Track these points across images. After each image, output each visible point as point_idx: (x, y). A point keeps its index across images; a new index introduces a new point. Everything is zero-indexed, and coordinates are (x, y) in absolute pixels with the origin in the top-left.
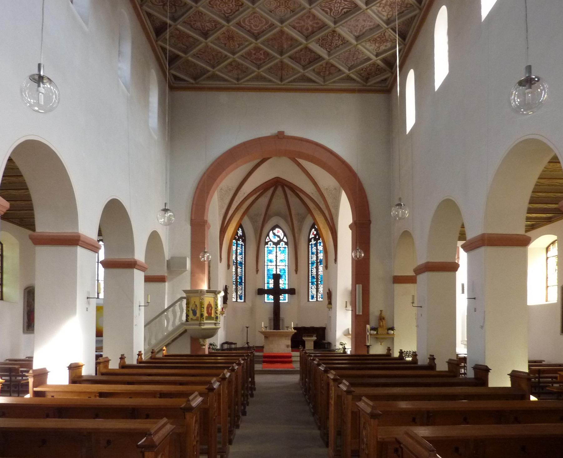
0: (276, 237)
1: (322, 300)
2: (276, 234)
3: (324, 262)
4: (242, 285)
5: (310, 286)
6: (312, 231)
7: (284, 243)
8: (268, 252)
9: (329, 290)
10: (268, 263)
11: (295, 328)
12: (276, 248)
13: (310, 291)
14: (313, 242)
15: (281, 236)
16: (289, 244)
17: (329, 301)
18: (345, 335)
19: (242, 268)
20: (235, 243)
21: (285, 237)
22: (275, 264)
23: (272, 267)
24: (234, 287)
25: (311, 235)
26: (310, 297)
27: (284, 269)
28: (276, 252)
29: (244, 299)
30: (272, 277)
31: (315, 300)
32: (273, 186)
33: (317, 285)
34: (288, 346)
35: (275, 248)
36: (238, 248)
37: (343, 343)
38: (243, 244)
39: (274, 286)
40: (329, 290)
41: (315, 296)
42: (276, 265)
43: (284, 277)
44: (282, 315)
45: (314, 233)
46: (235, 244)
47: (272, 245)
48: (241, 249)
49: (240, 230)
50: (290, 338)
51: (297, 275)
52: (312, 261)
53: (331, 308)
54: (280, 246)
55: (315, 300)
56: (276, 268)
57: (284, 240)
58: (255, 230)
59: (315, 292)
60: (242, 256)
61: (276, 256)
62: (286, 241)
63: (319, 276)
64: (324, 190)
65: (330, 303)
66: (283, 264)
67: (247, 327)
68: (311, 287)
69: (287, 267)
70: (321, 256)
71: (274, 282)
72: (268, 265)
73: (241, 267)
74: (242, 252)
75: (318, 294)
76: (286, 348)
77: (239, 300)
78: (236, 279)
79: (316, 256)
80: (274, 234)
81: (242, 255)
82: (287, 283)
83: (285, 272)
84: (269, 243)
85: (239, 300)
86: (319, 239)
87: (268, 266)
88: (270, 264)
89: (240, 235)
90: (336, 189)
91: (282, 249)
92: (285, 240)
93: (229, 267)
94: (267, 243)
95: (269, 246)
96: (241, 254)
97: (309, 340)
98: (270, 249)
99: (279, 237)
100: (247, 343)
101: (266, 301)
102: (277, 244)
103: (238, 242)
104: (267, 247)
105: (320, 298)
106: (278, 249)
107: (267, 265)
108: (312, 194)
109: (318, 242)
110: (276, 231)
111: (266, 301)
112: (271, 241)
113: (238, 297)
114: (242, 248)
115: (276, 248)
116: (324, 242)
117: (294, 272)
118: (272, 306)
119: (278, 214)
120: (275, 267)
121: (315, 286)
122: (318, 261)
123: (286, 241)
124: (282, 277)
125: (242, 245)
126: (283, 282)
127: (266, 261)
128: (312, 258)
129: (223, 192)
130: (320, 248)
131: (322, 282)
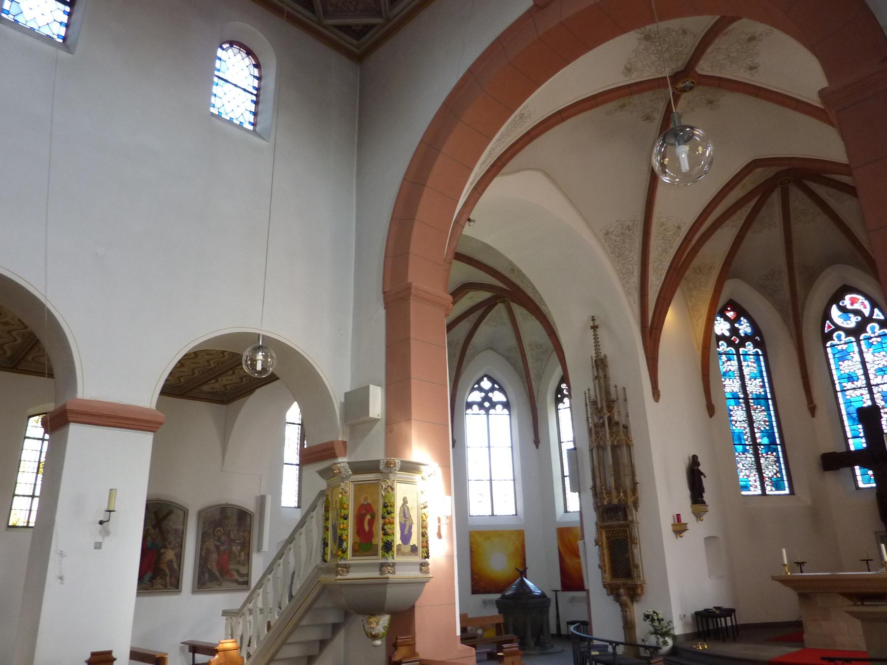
0: (851, 315)
2: (849, 307)
4: (776, 450)
8: (837, 356)
22: (864, 382)
23: (858, 392)
28: (861, 353)
35: (855, 344)
42: (869, 386)
48: (755, 365)
54: (869, 333)
56: (871, 393)
57: (874, 317)
61: (864, 363)
72: (845, 389)
77: (770, 490)
80: (843, 310)
82: (849, 440)
85: (770, 490)
87: (847, 393)
88: (849, 385)
92: (878, 315)
94: (828, 337)
98: (839, 348)
99: (857, 312)
102: (856, 332)
104: (832, 346)
106: (862, 343)
110: (847, 302)
112: (838, 328)
120: (865, 391)
125: (757, 354)
127: (837, 382)
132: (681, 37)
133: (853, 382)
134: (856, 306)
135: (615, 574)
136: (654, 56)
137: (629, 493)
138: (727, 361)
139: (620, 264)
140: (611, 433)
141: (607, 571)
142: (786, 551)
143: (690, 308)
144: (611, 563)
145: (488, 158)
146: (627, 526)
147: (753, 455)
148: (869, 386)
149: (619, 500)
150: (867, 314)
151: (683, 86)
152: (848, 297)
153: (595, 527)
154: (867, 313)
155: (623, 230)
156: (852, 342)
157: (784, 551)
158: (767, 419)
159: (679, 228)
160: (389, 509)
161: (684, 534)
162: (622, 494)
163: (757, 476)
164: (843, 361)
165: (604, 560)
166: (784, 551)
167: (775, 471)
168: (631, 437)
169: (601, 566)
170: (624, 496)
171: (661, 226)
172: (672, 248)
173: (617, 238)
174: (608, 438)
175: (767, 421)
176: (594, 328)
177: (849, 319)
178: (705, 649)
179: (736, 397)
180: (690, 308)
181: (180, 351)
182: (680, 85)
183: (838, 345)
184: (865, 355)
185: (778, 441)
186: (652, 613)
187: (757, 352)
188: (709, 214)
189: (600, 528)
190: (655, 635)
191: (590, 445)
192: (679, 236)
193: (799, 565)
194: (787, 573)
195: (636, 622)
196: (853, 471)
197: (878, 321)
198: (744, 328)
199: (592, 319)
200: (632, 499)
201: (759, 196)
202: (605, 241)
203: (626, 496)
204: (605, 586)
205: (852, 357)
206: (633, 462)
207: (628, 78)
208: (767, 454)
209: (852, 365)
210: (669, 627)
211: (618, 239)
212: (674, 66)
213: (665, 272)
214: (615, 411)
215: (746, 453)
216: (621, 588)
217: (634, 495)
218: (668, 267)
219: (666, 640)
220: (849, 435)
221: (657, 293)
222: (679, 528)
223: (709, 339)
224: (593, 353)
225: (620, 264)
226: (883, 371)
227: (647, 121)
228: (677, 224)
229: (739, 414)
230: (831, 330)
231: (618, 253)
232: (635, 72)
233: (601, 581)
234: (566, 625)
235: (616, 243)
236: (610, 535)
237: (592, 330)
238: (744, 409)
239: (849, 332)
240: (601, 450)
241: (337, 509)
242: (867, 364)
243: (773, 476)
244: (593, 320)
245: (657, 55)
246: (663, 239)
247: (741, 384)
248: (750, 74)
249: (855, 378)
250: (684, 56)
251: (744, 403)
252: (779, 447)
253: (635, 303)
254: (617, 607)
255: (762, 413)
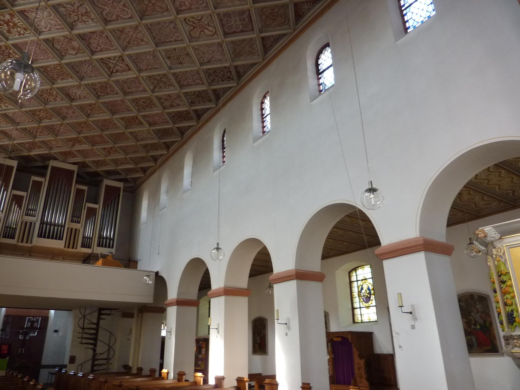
160: (504, 278)
181: (423, 193)
219: (99, 260)
234: (317, 86)
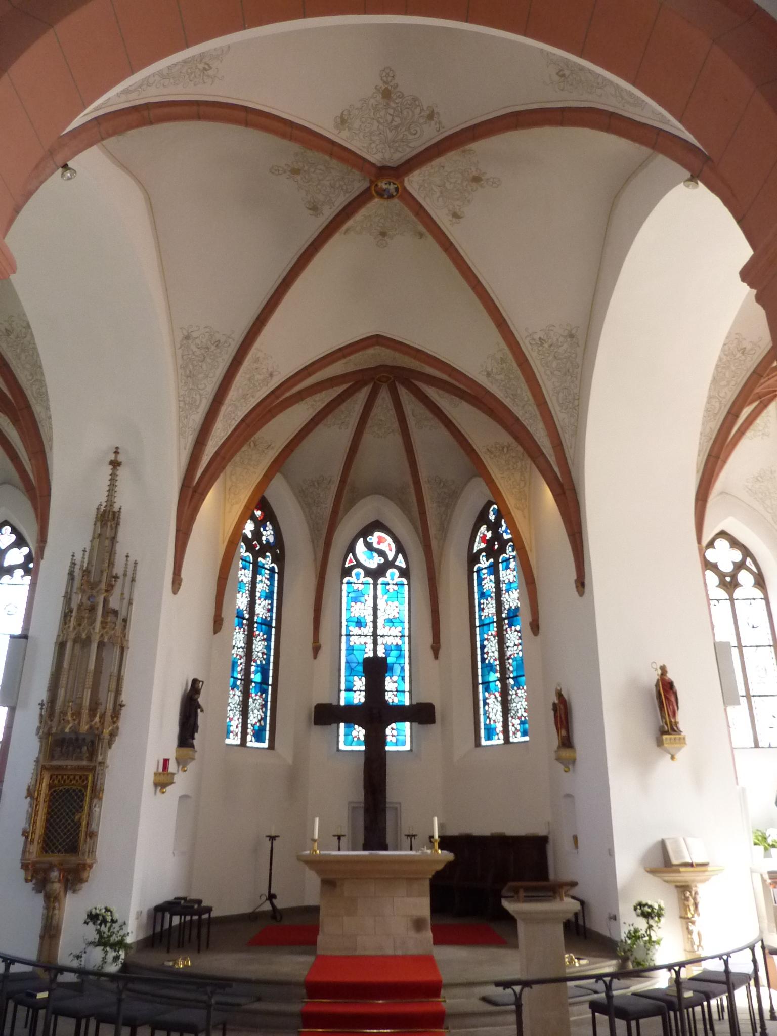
0: (375, 555)
1: (527, 738)
2: (375, 545)
3: (525, 618)
4: (265, 691)
5: (481, 697)
6: (479, 534)
7: (396, 572)
8: (351, 595)
9: (560, 695)
10: (351, 628)
11: (446, 842)
12: (375, 585)
13: (481, 711)
14: (484, 563)
15: (388, 552)
16: (414, 573)
17: (564, 733)
18: (653, 871)
19: (268, 640)
20: (250, 563)
21: (400, 556)
22: (371, 630)
23: (363, 640)
24: (235, 697)
25: (476, 544)
26: (482, 733)
27: (398, 647)
28: (375, 598)
29: (269, 740)
30: (360, 668)
31: (501, 741)
32: (365, 384)
33: (505, 692)
34: (418, 924)
35: (372, 586)
36: (259, 577)
37: (650, 907)
38: (276, 570)
39: (366, 697)
40: (560, 695)
41: (499, 727)
42: (375, 635)
43: (397, 669)
44: (395, 792)
45: (485, 536)
46: (251, 565)
47: (362, 579)
48: (268, 583)
49: (267, 528)
50: (427, 883)
51: (437, 662)
52: (483, 618)
53: (574, 761)
54: (387, 579)
55: (498, 740)
56: (375, 643)
57: (397, 563)
58: (314, 528)
59: (500, 714)
60: (270, 602)
61: (375, 609)
62: (403, 565)
63: (510, 661)
64: (530, 347)
65: (567, 742)
66: (396, 631)
67: (272, 838)
68: (485, 700)
69: (406, 639)
70: (512, 599)
71: (366, 686)
72: (351, 633)
73: (265, 636)
74: (272, 592)
75: (510, 719)
76: (412, 933)
77: (251, 743)
78: (247, 671)
79: (494, 602)
80: (369, 546)
81: (272, 599)
82: (408, 690)
83: (400, 656)
84: (354, 572)
85: (251, 743)
86: (503, 550)
87: (352, 639)
88: (355, 630)
89: (267, 541)
90: (571, 336)
91: (391, 587)
92: (401, 562)
93: (180, 585)
94: (347, 572)
95: (353, 579)
96: (269, 596)
97: (534, 919)
98: (355, 587)
99: (381, 553)
100: (271, 897)
101: (342, 747)
102: (376, 574)
103: (260, 559)
104: (349, 583)
105: (519, 734)
106: (379, 587)
107: (348, 635)
108: (488, 375)
109: (500, 561)
110: (374, 539)
111: (342, 747)
112: (359, 565)
113: (249, 731)
114: (271, 579)
115: (375, 585)
116: (519, 546)
117: (431, 653)
118: (361, 761)
119: (379, 489)
120: (370, 640)
121: (497, 694)
122: (504, 615)
123: (403, 565)
124: (392, 669)
125: (272, 570)
126: (396, 685)
127: (344, 623)
128: (482, 610)
129: (195, 349)
130: (508, 575)
131: (523, 679)
132: (421, 121)
133: (360, 628)
134: (383, 547)
135: (48, 845)
136: (377, 124)
137: (108, 719)
138: (242, 568)
139: (186, 388)
140: (104, 624)
141: (36, 843)
142: (438, 820)
143: (228, 487)
144: (46, 828)
145: (135, 90)
146: (93, 770)
147: (242, 693)
148: (375, 635)
149: (91, 728)
150: (391, 558)
151: (385, 186)
152: (377, 534)
153: (34, 767)
154: (391, 556)
155: (209, 342)
156: (369, 584)
157: (317, 820)
158: (265, 651)
159: (271, 375)
161: (168, 789)
162: (97, 719)
163: (240, 720)
164: (356, 603)
165: (35, 822)
166: (317, 820)
167: (259, 718)
168: (128, 636)
169: (28, 833)
170: (100, 722)
171: (255, 362)
172: (253, 397)
173: (196, 349)
174: (97, 630)
175: (265, 654)
176: (115, 464)
177: (372, 558)
178: (188, 966)
179: (240, 615)
180: (228, 487)
182: (383, 185)
183: (355, 583)
184: (379, 601)
185: (270, 682)
186: (103, 911)
187: (273, 567)
188: (310, 375)
189: (42, 768)
190: (102, 948)
191: (58, 636)
192: (267, 385)
193: (409, 838)
194: (315, 851)
195: (63, 926)
196: (338, 728)
197: (399, 568)
198: (268, 535)
199: (115, 450)
200: (110, 728)
201: (351, 384)
202: (181, 347)
203: (102, 723)
204: (25, 866)
205: (366, 601)
206: (122, 675)
207: (336, 132)
208: (256, 695)
209: (364, 610)
210: (122, 933)
211: (198, 352)
212: (387, 156)
213: (235, 424)
214: (117, 591)
215: (235, 689)
216: (55, 869)
217: (114, 723)
218: (241, 419)
220: (343, 687)
221: (217, 448)
222: (163, 781)
223: (237, 536)
224: (103, 499)
225: (186, 388)
226: (392, 622)
227: (311, 212)
228: (270, 370)
229: (239, 639)
230: (352, 566)
231: (190, 372)
232: (347, 129)
233: (19, 857)
235: (194, 357)
236: (56, 782)
237: (112, 467)
238: (246, 633)
239: (369, 572)
240: (78, 647)
241: (413, 416)
242: (378, 611)
243: (256, 723)
244: (116, 453)
245: (381, 127)
246: (249, 379)
247: (250, 601)
248: (450, 220)
249: (363, 624)
250: (408, 150)
251: (248, 625)
252: (270, 688)
253: (185, 448)
254: (39, 901)
255: (263, 642)
